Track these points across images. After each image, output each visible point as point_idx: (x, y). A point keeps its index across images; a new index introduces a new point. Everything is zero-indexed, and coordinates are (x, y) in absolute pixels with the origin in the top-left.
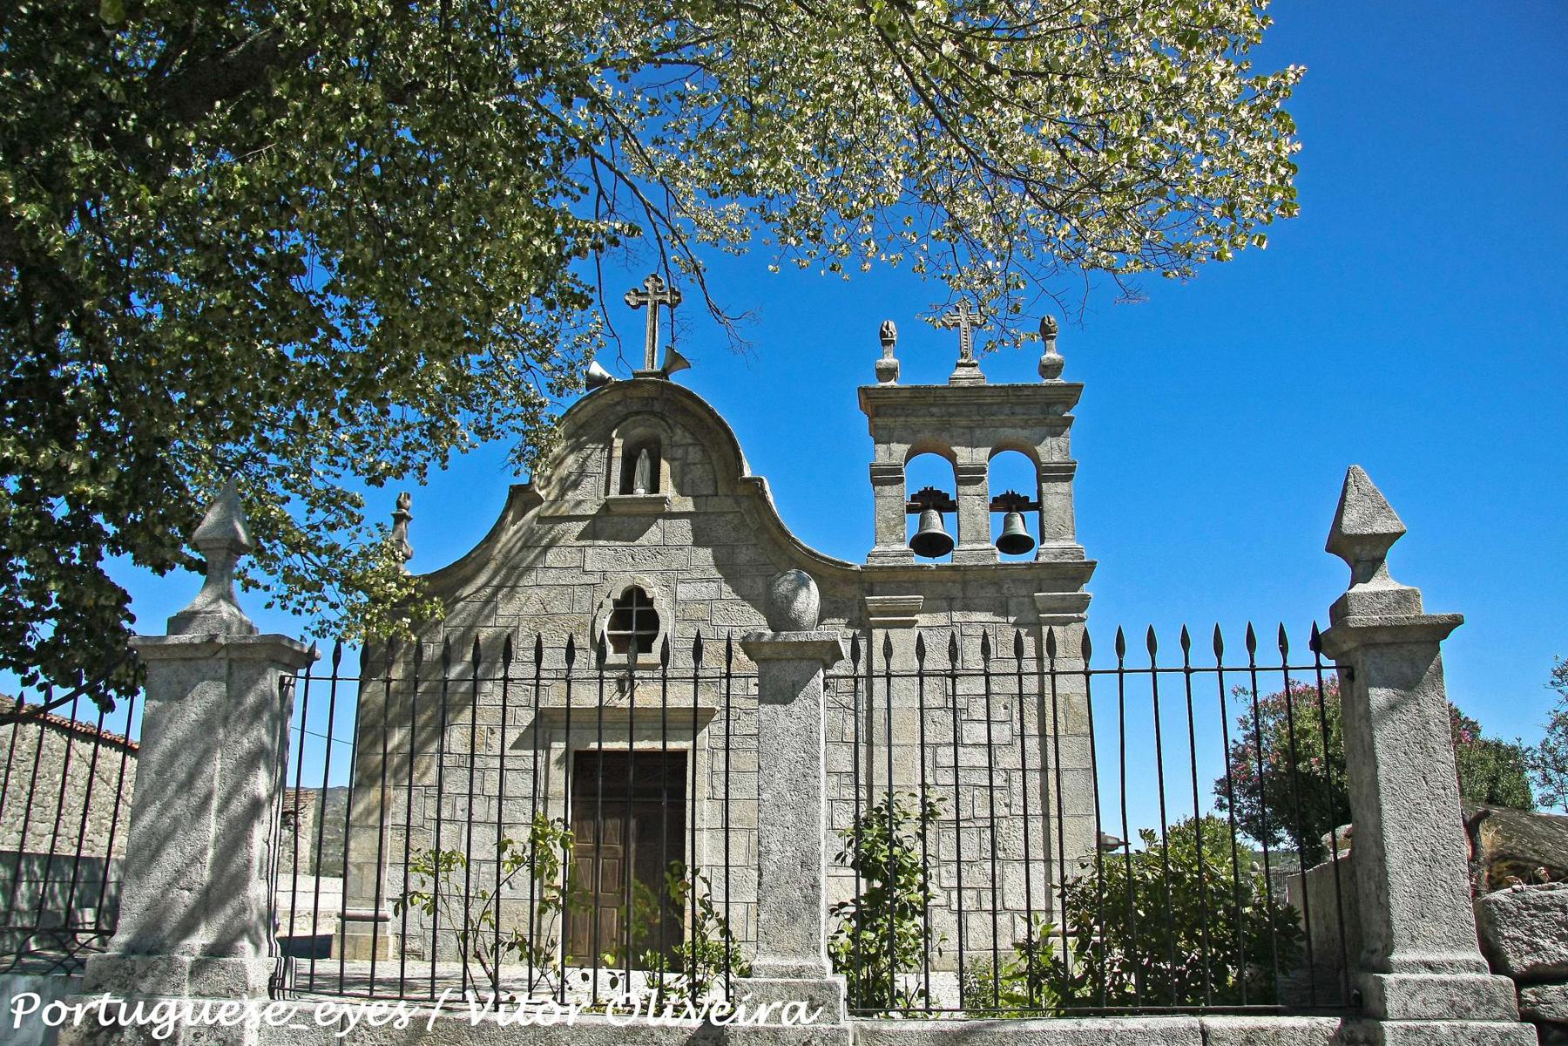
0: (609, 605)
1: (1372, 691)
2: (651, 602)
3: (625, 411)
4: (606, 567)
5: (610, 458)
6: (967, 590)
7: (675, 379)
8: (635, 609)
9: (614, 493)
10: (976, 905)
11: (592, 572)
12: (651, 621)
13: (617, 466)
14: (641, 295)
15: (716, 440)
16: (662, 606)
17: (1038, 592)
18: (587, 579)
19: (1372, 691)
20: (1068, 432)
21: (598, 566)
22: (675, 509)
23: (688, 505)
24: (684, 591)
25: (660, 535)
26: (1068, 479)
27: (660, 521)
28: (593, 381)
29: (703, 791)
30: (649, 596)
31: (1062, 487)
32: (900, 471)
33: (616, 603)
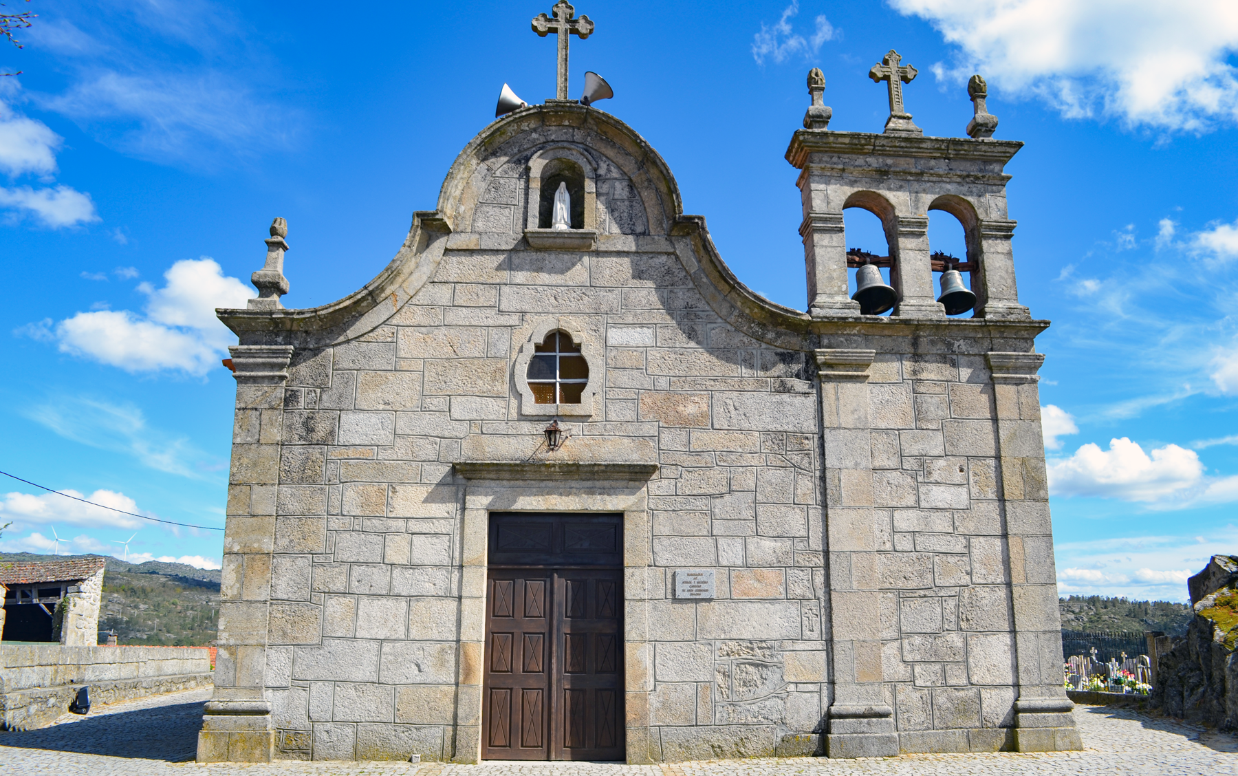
0: (530, 351)
1: (970, 371)
2: (578, 348)
3: (542, 139)
4: (526, 307)
5: (527, 189)
6: (916, 342)
7: (599, 106)
8: (558, 354)
9: (533, 225)
10: (948, 668)
11: (509, 313)
12: (579, 368)
13: (535, 198)
14: (550, 20)
15: (649, 175)
16: (590, 353)
17: (983, 338)
18: (504, 320)
19: (970, 371)
20: (1004, 191)
21: (515, 306)
22: (603, 248)
23: (630, 244)
24: (616, 336)
25: (586, 275)
26: (1008, 237)
27: (586, 259)
28: (504, 108)
29: (1124, 540)
30: (576, 340)
31: (1002, 246)
32: (840, 220)
33: (538, 348)
